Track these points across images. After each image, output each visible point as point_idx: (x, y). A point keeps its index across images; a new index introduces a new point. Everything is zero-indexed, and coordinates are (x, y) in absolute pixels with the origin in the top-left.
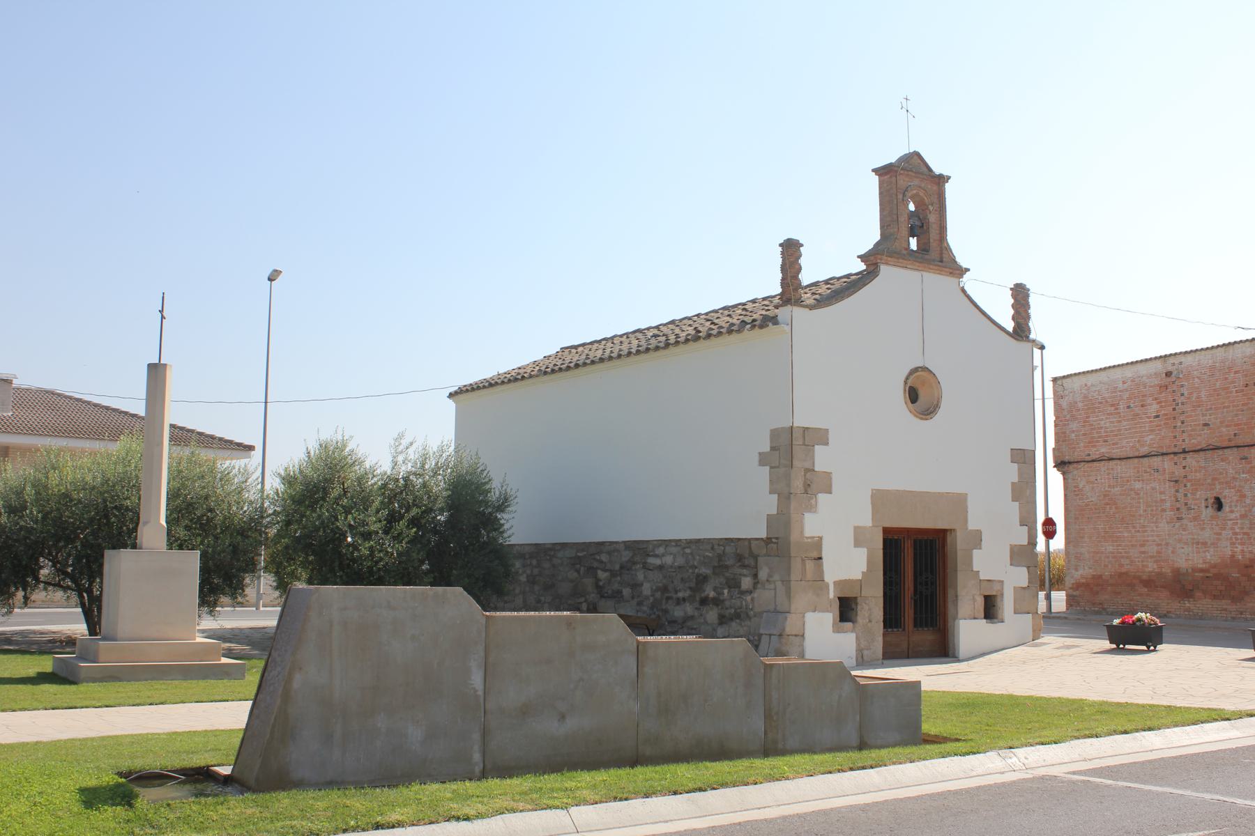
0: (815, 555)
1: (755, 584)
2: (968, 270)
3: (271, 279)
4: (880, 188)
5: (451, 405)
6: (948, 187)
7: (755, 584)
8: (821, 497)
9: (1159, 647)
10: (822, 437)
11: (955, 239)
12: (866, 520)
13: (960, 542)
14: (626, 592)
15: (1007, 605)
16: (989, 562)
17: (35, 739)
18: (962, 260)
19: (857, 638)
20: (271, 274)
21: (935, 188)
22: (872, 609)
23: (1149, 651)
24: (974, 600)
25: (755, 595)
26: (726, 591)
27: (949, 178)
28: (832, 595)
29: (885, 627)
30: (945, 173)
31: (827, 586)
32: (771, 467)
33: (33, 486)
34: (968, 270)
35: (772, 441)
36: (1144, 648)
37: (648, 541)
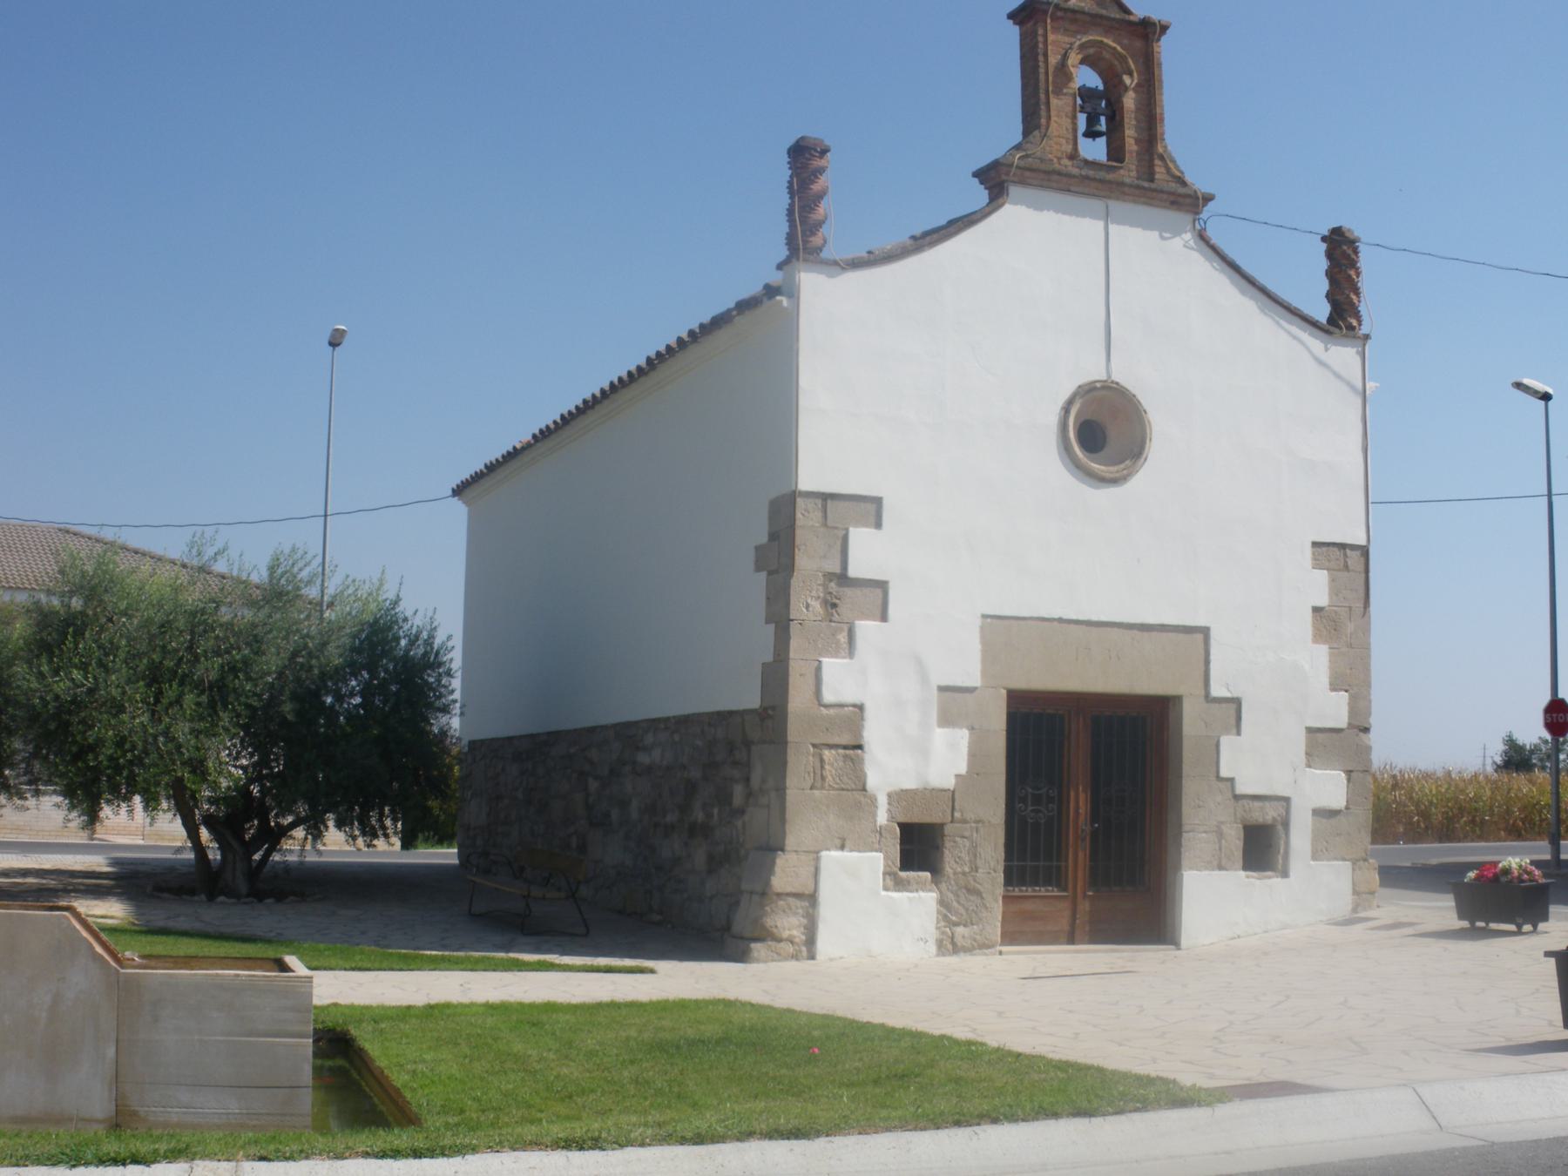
0: (845, 739)
1: (749, 795)
2: (1208, 198)
3: (334, 344)
4: (1022, 46)
5: (458, 510)
6: (1167, 49)
7: (749, 795)
8: (866, 629)
9: (1542, 926)
10: (871, 509)
11: (1176, 138)
12: (969, 671)
13: (1192, 721)
14: (615, 814)
15: (1300, 838)
16: (1261, 752)
17: (971, 1036)
18: (1198, 180)
19: (942, 902)
20: (332, 336)
21: (1138, 44)
22: (980, 848)
23: (1519, 933)
24: (1220, 835)
25: (746, 818)
26: (716, 811)
27: (1164, 28)
28: (882, 817)
29: (1009, 880)
30: (1155, 16)
31: (873, 801)
32: (770, 573)
33: (295, 697)
34: (1208, 198)
35: (770, 525)
36: (1512, 927)
37: (636, 723)
